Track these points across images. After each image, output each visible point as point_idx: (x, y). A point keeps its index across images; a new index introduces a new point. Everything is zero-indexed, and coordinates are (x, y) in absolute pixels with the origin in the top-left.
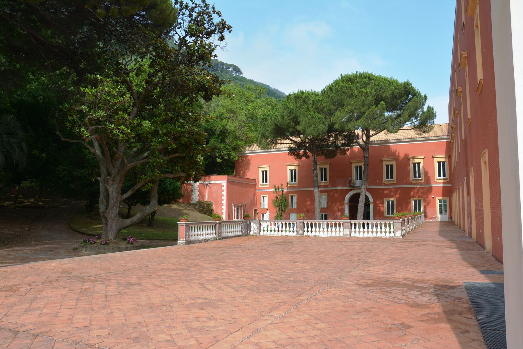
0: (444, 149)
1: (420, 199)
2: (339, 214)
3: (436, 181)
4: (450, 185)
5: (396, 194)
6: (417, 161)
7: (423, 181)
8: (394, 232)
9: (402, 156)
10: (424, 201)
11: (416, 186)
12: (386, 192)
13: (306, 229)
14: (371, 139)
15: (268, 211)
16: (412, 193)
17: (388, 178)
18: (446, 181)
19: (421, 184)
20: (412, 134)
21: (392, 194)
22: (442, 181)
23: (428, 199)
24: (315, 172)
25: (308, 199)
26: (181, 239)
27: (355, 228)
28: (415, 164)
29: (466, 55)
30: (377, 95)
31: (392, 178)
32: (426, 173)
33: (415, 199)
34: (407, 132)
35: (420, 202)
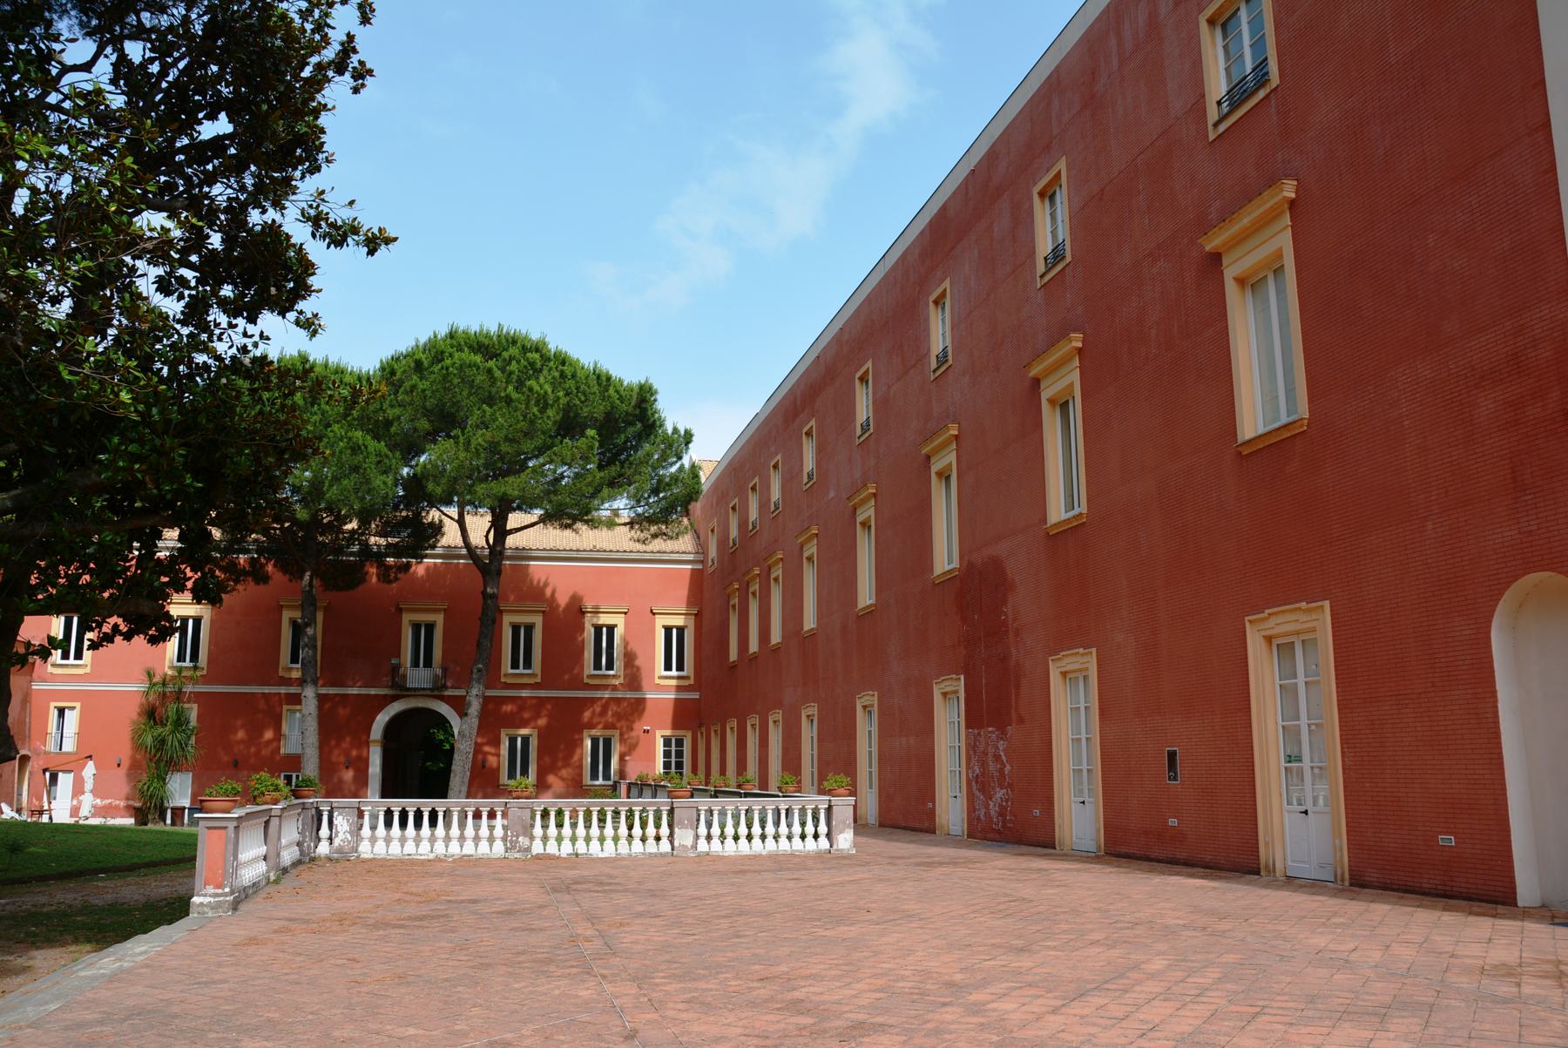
0: (683, 591)
1: (608, 733)
2: (348, 775)
3: (657, 681)
4: (696, 695)
5: (537, 716)
6: (605, 619)
7: (621, 680)
8: (828, 836)
9: (563, 600)
10: (622, 740)
11: (598, 694)
12: (508, 708)
13: (703, 830)
14: (511, 541)
15: (91, 764)
16: (587, 715)
17: (515, 665)
18: (686, 683)
19: (614, 688)
20: (620, 539)
21: (526, 715)
22: (674, 682)
23: (633, 734)
24: (310, 631)
25: (239, 723)
26: (210, 890)
27: (560, 825)
28: (598, 629)
29: (1080, 345)
30: (568, 409)
31: (528, 665)
32: (629, 658)
33: (594, 732)
34: (612, 534)
35: (608, 743)
